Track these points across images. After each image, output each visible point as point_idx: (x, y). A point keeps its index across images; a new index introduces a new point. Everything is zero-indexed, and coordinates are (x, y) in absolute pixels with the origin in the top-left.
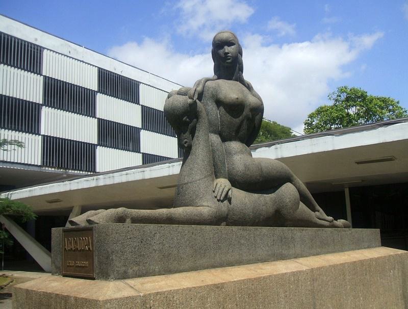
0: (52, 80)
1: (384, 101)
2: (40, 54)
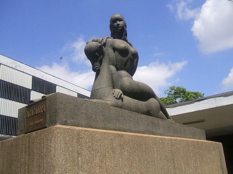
1: (196, 94)
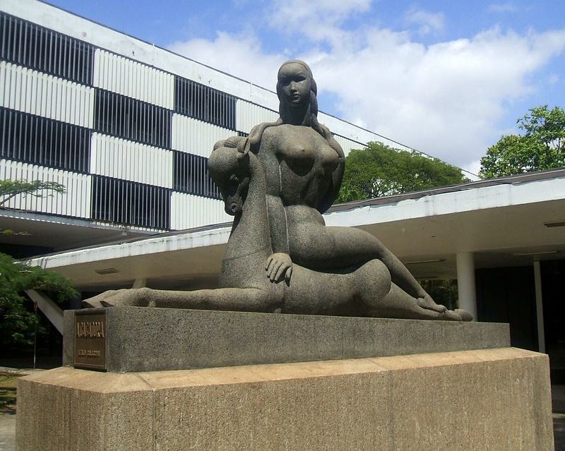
0: (107, 94)
2: (91, 55)
